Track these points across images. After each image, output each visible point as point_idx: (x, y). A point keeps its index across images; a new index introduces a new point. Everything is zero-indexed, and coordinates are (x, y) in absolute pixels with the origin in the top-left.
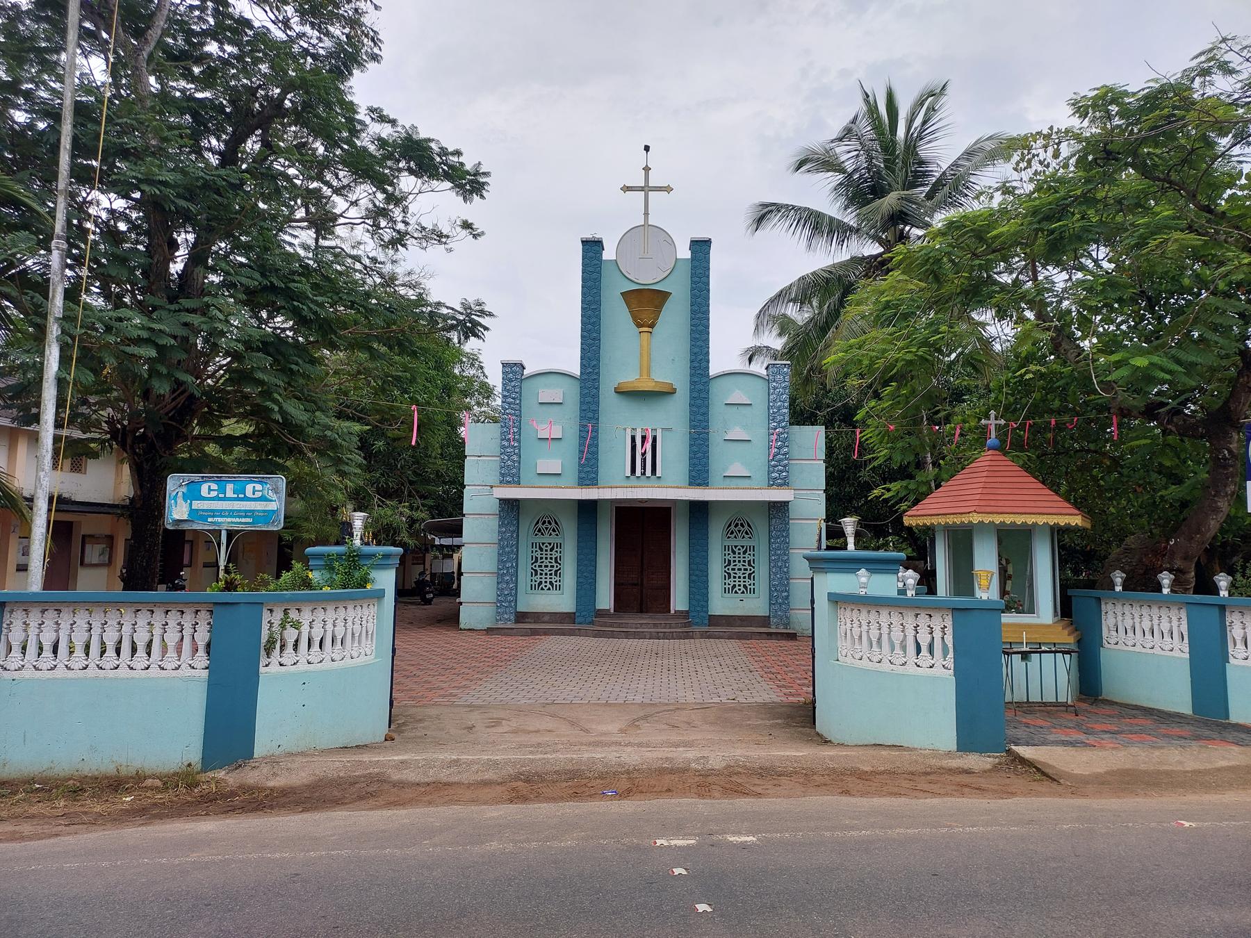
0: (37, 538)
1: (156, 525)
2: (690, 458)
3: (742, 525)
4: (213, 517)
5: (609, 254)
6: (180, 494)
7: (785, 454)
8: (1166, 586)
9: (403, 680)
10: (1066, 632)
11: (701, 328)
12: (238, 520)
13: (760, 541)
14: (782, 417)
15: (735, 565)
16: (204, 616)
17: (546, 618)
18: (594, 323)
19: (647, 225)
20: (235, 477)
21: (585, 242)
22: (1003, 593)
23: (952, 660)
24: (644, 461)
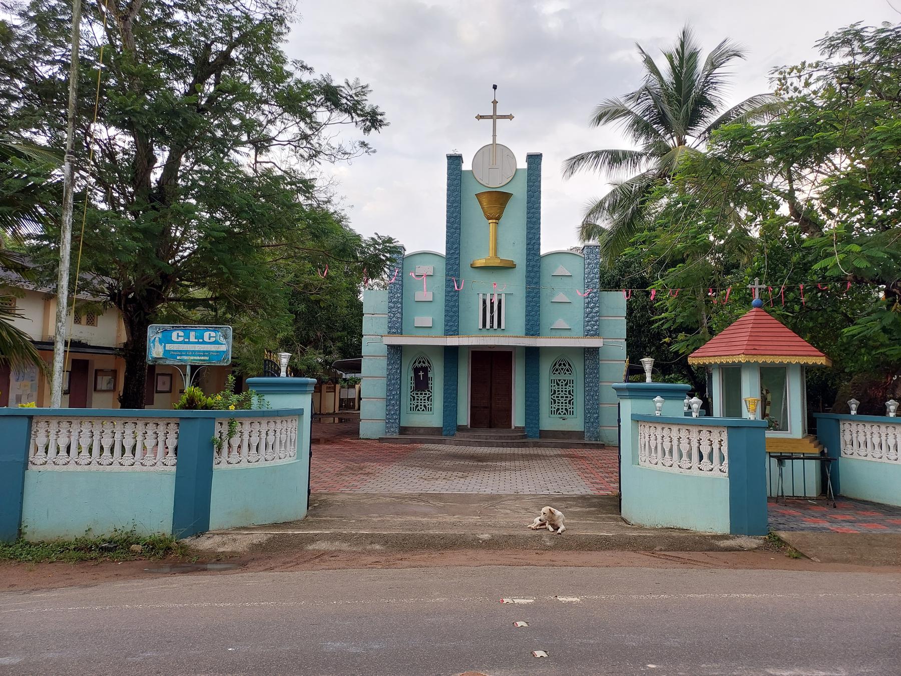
0: (58, 370)
1: (144, 362)
2: (527, 316)
3: (424, 362)
4: (181, 355)
5: (467, 166)
6: (157, 339)
7: (596, 312)
8: (854, 409)
9: (318, 474)
10: (813, 445)
11: (534, 220)
12: (198, 358)
13: (578, 374)
14: (594, 285)
15: (559, 394)
16: (173, 427)
17: (422, 431)
18: (535, 222)
19: (494, 144)
20: (196, 327)
21: (450, 157)
22: (764, 415)
23: (727, 465)
24: (492, 317)
